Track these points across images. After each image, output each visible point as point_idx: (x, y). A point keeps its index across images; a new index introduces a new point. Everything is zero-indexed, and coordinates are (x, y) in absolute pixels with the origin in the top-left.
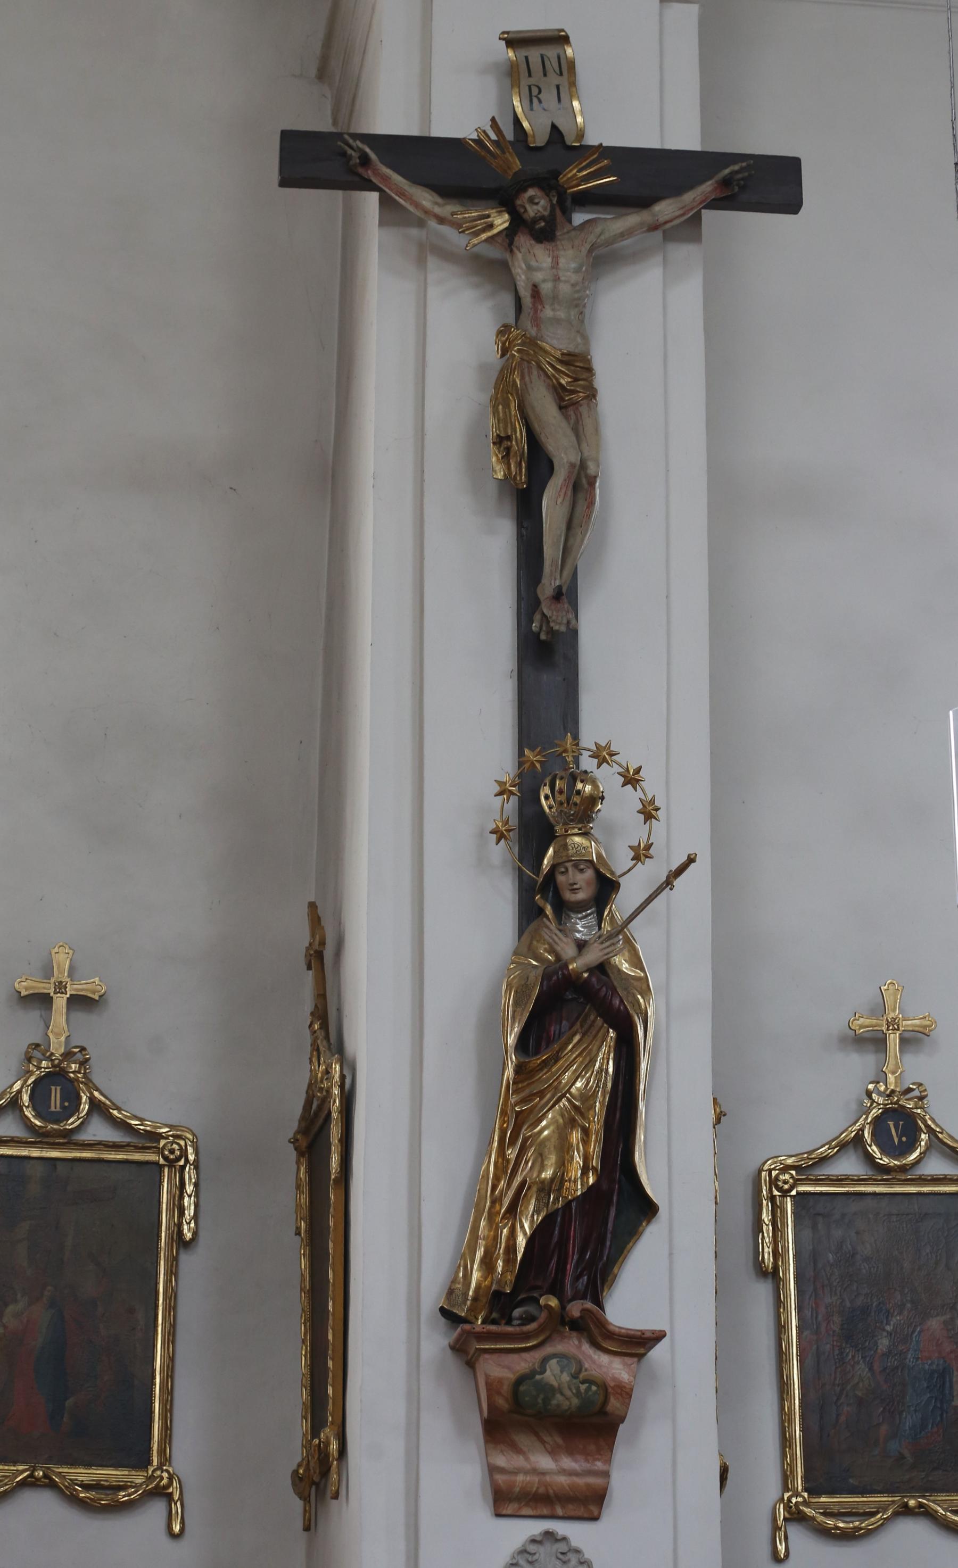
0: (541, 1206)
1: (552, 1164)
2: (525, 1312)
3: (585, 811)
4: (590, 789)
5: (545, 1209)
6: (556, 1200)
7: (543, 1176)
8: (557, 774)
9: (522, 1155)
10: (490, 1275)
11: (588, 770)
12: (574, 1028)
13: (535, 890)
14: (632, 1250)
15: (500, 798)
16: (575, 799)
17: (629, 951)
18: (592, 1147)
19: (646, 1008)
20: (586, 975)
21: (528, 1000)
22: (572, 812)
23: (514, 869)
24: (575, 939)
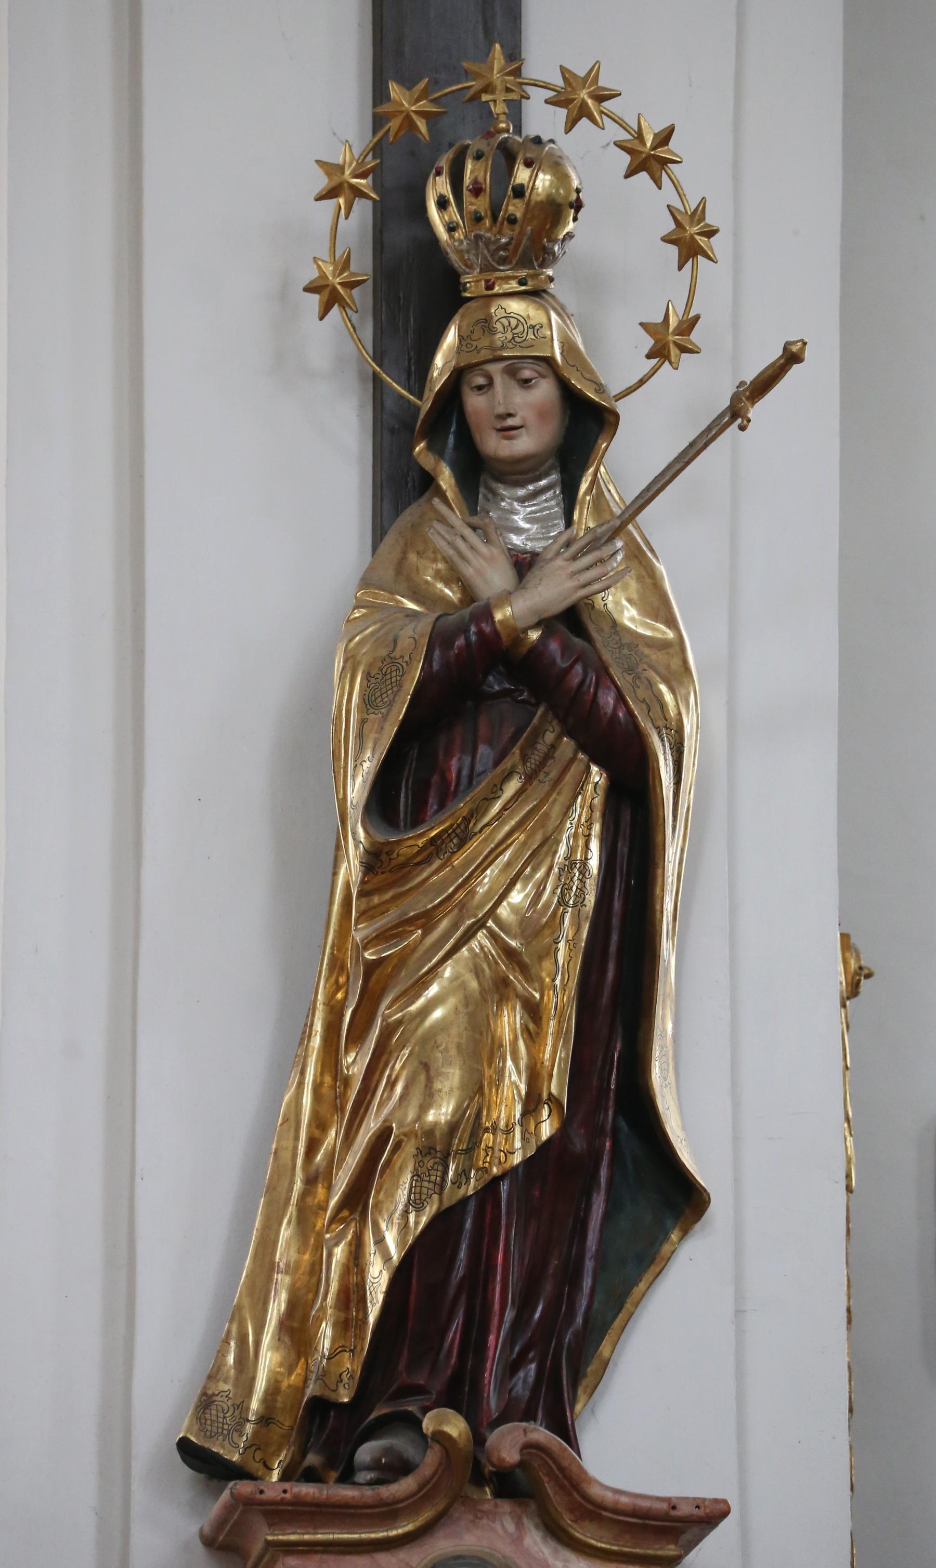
0: (425, 1190)
1: (451, 1090)
2: (387, 1451)
3: (536, 238)
4: (547, 183)
5: (436, 1197)
6: (464, 1175)
7: (431, 1117)
8: (469, 145)
9: (381, 1065)
10: (303, 1360)
11: (542, 137)
12: (505, 760)
13: (413, 431)
14: (644, 1300)
15: (330, 204)
16: (511, 208)
17: (639, 579)
18: (549, 1048)
19: (680, 714)
20: (534, 635)
21: (395, 695)
22: (503, 240)
23: (362, 378)
24: (509, 549)
